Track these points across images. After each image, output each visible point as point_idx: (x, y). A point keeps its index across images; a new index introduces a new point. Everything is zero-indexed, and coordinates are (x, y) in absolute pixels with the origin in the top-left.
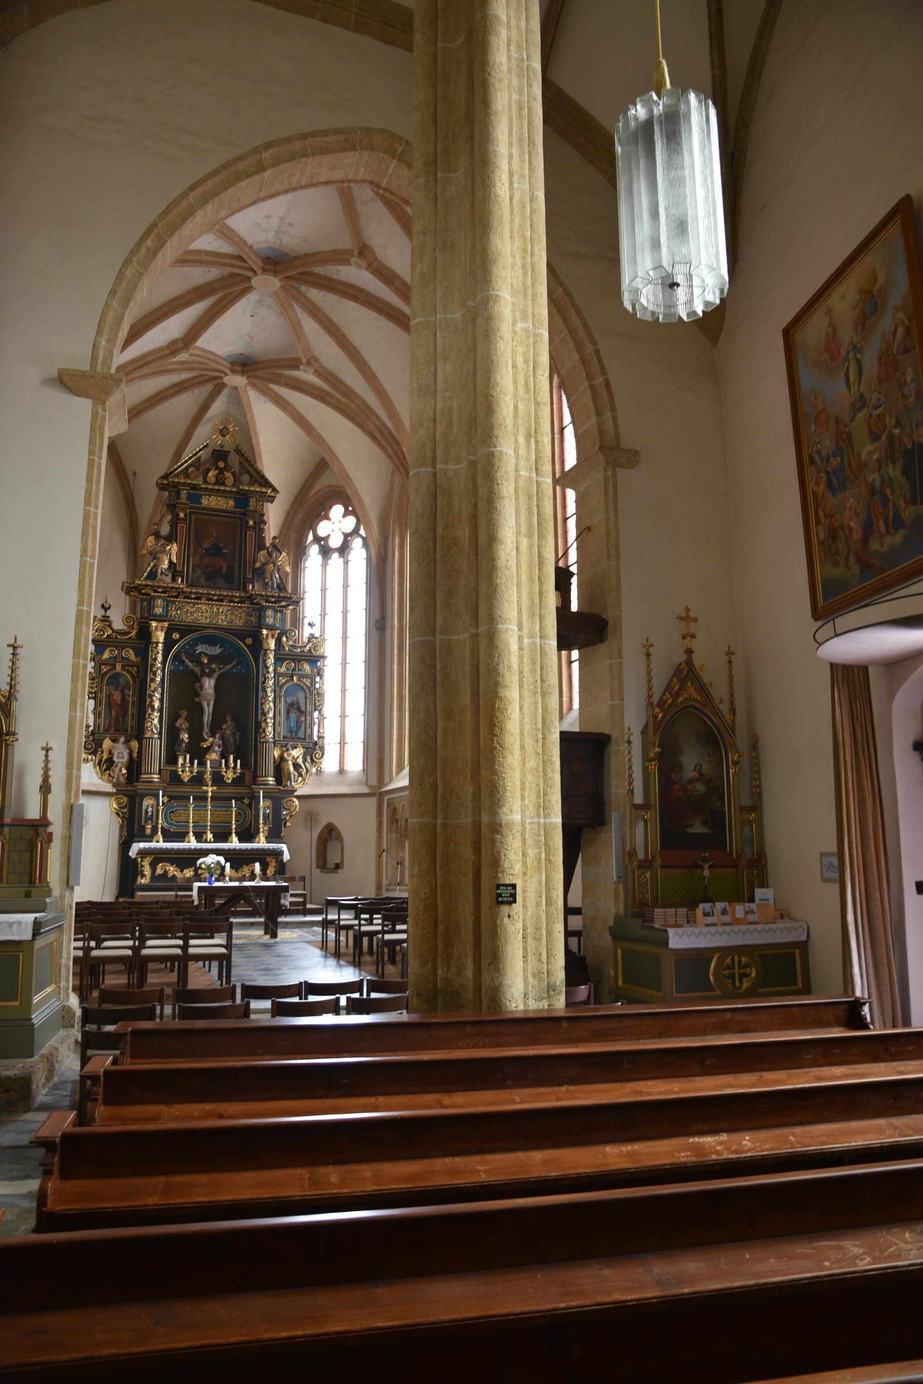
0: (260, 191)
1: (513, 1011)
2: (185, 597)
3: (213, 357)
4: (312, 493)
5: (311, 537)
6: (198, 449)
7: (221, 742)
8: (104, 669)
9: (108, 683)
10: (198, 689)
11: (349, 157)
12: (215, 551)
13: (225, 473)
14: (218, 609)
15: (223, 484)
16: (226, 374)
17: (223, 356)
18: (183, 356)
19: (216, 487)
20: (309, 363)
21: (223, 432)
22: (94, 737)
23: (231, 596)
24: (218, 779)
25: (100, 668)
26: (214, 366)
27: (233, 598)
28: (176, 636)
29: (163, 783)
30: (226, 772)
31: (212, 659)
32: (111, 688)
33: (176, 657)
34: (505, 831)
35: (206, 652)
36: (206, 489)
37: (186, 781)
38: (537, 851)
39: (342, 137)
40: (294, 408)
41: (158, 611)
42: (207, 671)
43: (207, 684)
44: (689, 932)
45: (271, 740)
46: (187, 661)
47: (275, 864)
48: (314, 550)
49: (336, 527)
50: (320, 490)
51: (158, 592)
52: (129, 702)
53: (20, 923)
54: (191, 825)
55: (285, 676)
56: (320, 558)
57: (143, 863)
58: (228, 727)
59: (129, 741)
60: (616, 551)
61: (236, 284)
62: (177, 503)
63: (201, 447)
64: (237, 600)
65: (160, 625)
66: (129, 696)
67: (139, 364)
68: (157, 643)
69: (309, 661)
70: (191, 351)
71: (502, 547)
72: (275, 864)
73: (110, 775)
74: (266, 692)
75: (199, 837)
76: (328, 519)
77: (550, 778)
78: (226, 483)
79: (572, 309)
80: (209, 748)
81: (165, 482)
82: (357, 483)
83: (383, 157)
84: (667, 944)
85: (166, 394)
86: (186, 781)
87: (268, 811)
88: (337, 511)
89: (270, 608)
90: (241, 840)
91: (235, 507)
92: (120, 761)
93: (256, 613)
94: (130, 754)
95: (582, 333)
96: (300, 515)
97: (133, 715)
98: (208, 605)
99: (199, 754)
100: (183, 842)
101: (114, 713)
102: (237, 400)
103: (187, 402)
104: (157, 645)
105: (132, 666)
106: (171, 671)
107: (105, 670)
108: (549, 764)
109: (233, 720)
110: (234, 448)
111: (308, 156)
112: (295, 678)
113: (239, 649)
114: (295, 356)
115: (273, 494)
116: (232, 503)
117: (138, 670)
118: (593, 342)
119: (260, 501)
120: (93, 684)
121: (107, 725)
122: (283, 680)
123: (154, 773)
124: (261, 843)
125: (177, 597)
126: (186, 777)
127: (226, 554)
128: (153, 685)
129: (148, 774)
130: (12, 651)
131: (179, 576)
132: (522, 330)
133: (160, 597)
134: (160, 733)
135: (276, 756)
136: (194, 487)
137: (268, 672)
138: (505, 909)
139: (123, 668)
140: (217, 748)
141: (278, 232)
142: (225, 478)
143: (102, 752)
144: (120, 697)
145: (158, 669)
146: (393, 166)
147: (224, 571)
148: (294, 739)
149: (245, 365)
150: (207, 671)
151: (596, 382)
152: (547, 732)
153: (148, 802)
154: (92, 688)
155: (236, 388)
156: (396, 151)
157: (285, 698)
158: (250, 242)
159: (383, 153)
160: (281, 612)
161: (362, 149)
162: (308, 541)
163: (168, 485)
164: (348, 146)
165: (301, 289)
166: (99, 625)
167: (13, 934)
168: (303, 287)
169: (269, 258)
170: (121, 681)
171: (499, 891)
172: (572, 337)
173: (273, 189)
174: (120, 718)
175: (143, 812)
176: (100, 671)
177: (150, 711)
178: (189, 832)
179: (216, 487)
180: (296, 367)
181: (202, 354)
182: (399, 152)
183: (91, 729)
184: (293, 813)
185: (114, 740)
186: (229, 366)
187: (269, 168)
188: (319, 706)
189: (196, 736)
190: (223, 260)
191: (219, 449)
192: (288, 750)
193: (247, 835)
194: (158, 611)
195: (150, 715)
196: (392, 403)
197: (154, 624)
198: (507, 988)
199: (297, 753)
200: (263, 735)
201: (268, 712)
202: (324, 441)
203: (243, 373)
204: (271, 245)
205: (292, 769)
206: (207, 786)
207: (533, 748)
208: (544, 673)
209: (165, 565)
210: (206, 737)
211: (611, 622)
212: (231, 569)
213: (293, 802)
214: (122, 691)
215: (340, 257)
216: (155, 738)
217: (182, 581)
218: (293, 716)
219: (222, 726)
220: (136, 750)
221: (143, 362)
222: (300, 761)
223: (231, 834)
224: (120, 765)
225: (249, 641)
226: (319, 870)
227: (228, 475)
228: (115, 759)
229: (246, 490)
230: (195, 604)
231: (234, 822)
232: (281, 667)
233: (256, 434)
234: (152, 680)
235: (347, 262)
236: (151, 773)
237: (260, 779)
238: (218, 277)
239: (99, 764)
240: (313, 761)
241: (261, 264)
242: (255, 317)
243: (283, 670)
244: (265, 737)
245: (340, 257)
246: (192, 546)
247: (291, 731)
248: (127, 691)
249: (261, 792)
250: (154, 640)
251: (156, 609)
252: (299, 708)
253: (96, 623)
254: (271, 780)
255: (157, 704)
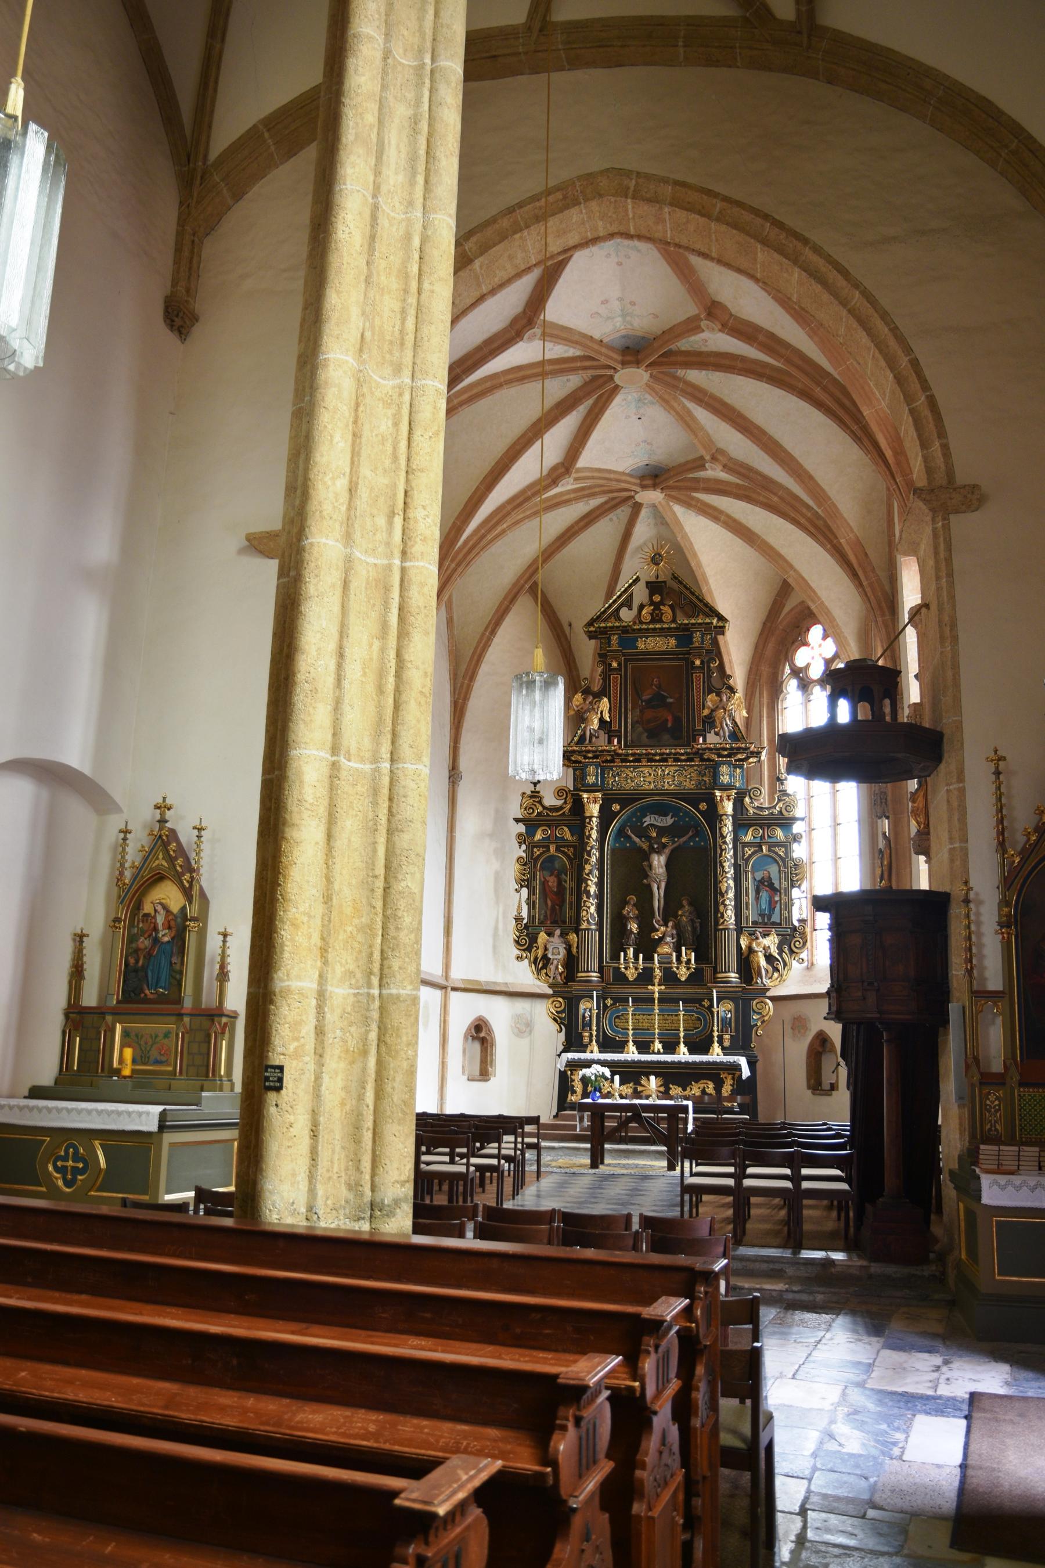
0: (479, 285)
1: (274, 1223)
2: (623, 761)
3: (612, 476)
4: (782, 615)
5: (787, 670)
6: (627, 585)
7: (675, 932)
8: (537, 852)
9: (542, 868)
10: (647, 869)
11: (575, 215)
12: (658, 701)
13: (662, 607)
14: (663, 771)
15: (661, 621)
16: (636, 493)
17: (627, 471)
18: (567, 485)
19: (651, 626)
20: (714, 458)
21: (656, 559)
22: (528, 930)
23: (675, 754)
24: (670, 977)
25: (532, 851)
26: (616, 485)
27: (678, 756)
28: (616, 807)
29: (602, 982)
30: (678, 968)
31: (662, 831)
32: (546, 873)
33: (621, 833)
34: (278, 999)
35: (655, 823)
36: (640, 629)
37: (683, 979)
38: (363, 1030)
39: (559, 195)
40: (728, 516)
41: (591, 779)
42: (656, 846)
43: (655, 863)
44: (1032, 1183)
45: (731, 927)
46: (633, 836)
47: (731, 1082)
48: (792, 686)
49: (816, 652)
50: (792, 610)
51: (589, 758)
52: (566, 888)
53: (148, 1113)
54: (631, 1032)
55: (751, 846)
56: (800, 693)
57: (573, 1077)
58: (685, 914)
59: (567, 934)
60: (951, 630)
61: (600, 387)
62: (609, 651)
63: (631, 581)
64: (683, 758)
65: (592, 795)
66: (566, 882)
67: (518, 501)
68: (591, 817)
69: (780, 825)
70: (574, 475)
71: (304, 657)
72: (731, 1082)
73: (547, 974)
74: (723, 867)
75: (643, 1047)
76: (806, 644)
77: (394, 938)
78: (664, 619)
79: (876, 315)
80: (661, 939)
81: (592, 629)
82: (823, 594)
83: (616, 201)
84: (979, 1198)
85: (576, 528)
86: (683, 979)
87: (729, 1016)
88: (815, 633)
89: (724, 763)
90: (692, 1051)
91: (677, 646)
92: (555, 957)
93: (709, 772)
94: (569, 949)
95: (892, 343)
96: (770, 646)
97: (571, 903)
98: (651, 767)
99: (647, 947)
100: (622, 1052)
101: (549, 903)
102: (660, 519)
103: (606, 530)
104: (591, 820)
105: (568, 846)
106: (613, 851)
107: (538, 853)
108: (392, 920)
109: (690, 904)
110: (670, 576)
111: (521, 230)
112: (764, 847)
113: (693, 817)
114: (697, 455)
115: (720, 624)
116: (673, 642)
117: (575, 851)
118: (908, 350)
119: (707, 634)
120: (525, 870)
121: (542, 917)
122: (749, 851)
123: (591, 971)
124: (716, 1055)
125: (612, 761)
126: (631, 974)
127: (671, 703)
128: (588, 867)
129: (584, 972)
130: (197, 834)
131: (615, 736)
132: (393, 388)
133: (591, 764)
134: (600, 925)
135: (743, 947)
136: (625, 630)
137: (725, 843)
138: (272, 1096)
139: (558, 849)
140: (668, 939)
141: (624, 315)
142: (662, 614)
143: (538, 948)
144: (555, 884)
145: (592, 848)
146: (630, 207)
147: (669, 725)
148: (766, 924)
149: (656, 476)
150: (656, 846)
151: (918, 404)
152: (392, 880)
153: (583, 1005)
154: (524, 875)
155: (654, 506)
156: (628, 188)
157: (753, 874)
158: (597, 336)
159: (613, 196)
160: (741, 767)
161: (586, 200)
162: (786, 675)
163: (595, 632)
164: (569, 202)
165: (678, 374)
166: (528, 802)
167: (142, 1124)
168: (680, 371)
169: (628, 348)
170: (557, 865)
171: (267, 1074)
172: (881, 351)
173: (496, 280)
174: (557, 907)
175: (580, 1017)
176: (532, 854)
177: (585, 899)
178: (628, 1041)
179: (651, 626)
180: (702, 467)
181: (596, 474)
182: (632, 188)
183: (525, 921)
184: (766, 1018)
185: (550, 934)
186: (638, 481)
187: (476, 258)
188: (797, 881)
189: (647, 927)
190: (572, 365)
191: (655, 580)
192: (757, 938)
193: (700, 1045)
194: (591, 779)
195: (585, 901)
196: (818, 485)
197: (585, 796)
198: (267, 1194)
199: (771, 942)
200: (722, 921)
201: (727, 892)
202: (772, 548)
203: (654, 486)
204: (624, 332)
205: (763, 962)
206: (654, 985)
207: (368, 898)
208: (394, 805)
209: (595, 724)
210: (657, 926)
211: (947, 732)
212: (677, 720)
213: (766, 1004)
214: (558, 877)
215: (691, 326)
216: (592, 930)
217: (619, 742)
218: (764, 895)
219: (677, 912)
220: (576, 945)
221: (521, 499)
222: (774, 952)
223: (679, 1043)
224: (555, 962)
225: (703, 806)
226: (809, 1092)
227: (666, 609)
228: (550, 956)
229: (604, 628)
230: (635, 767)
231: (682, 1029)
232: (746, 836)
233: (695, 555)
234: (587, 861)
235: (698, 329)
236: (588, 971)
237: (720, 975)
238: (580, 384)
239: (535, 962)
240: (792, 952)
241: (620, 358)
242: (643, 418)
243: (748, 838)
244: (723, 923)
245: (691, 326)
246: (630, 698)
247: (762, 915)
248: (563, 876)
249: (714, 991)
250: (587, 814)
251: (588, 778)
252: (771, 886)
253: (524, 801)
254: (733, 977)
255: (593, 889)
